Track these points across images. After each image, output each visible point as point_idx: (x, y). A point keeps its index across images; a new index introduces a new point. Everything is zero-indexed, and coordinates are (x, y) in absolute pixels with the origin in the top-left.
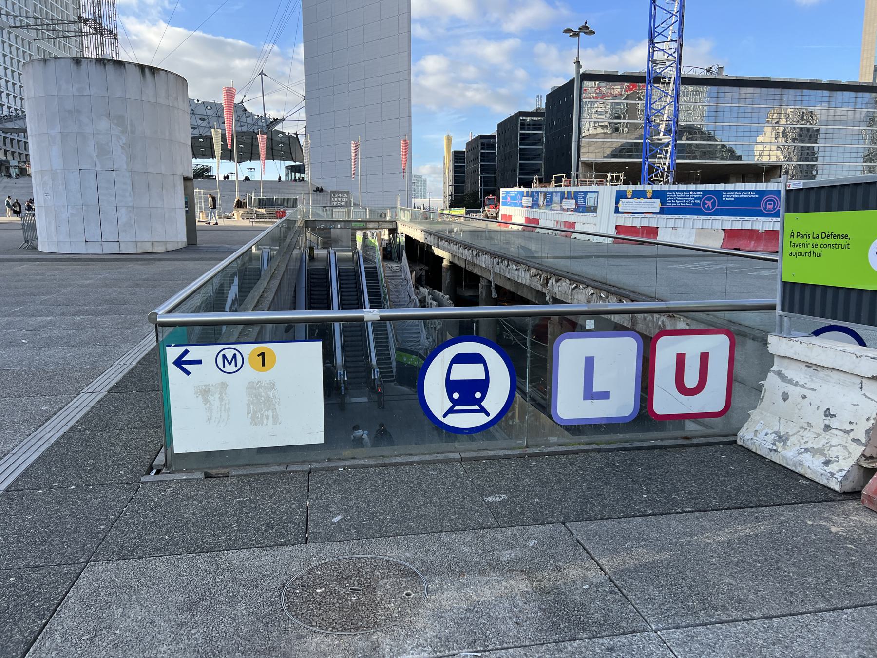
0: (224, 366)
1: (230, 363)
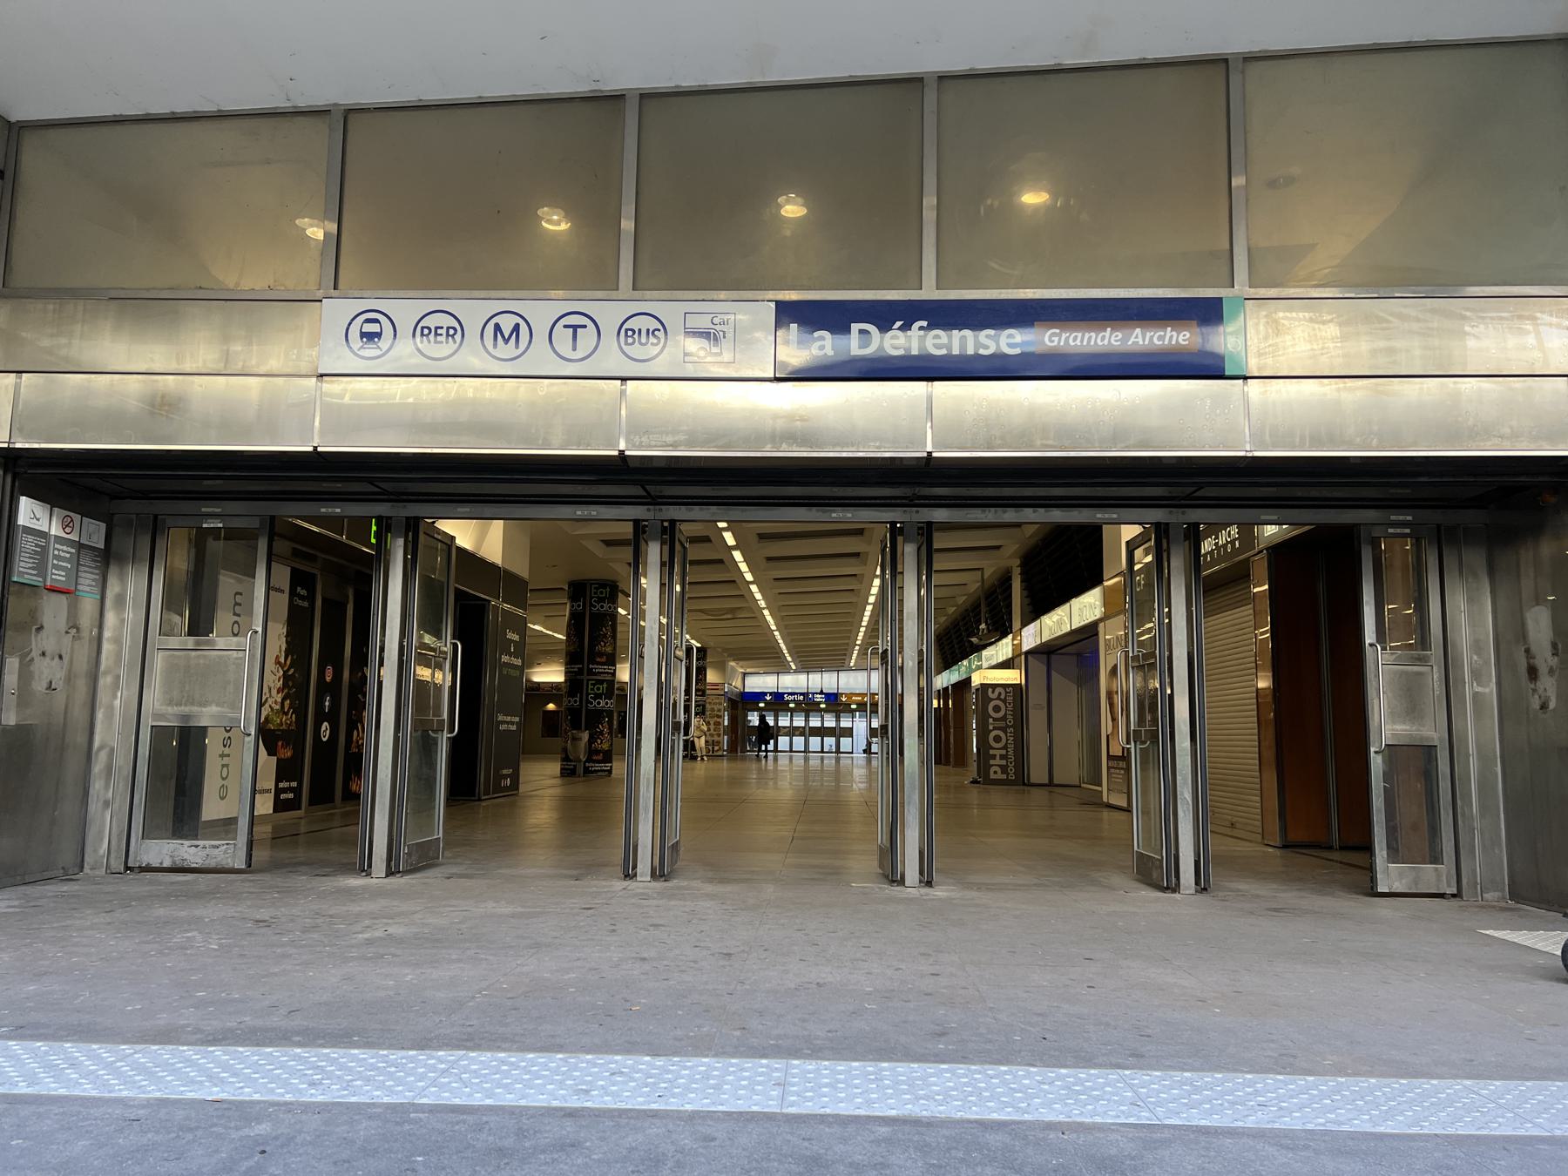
0: (495, 346)
1: (506, 341)
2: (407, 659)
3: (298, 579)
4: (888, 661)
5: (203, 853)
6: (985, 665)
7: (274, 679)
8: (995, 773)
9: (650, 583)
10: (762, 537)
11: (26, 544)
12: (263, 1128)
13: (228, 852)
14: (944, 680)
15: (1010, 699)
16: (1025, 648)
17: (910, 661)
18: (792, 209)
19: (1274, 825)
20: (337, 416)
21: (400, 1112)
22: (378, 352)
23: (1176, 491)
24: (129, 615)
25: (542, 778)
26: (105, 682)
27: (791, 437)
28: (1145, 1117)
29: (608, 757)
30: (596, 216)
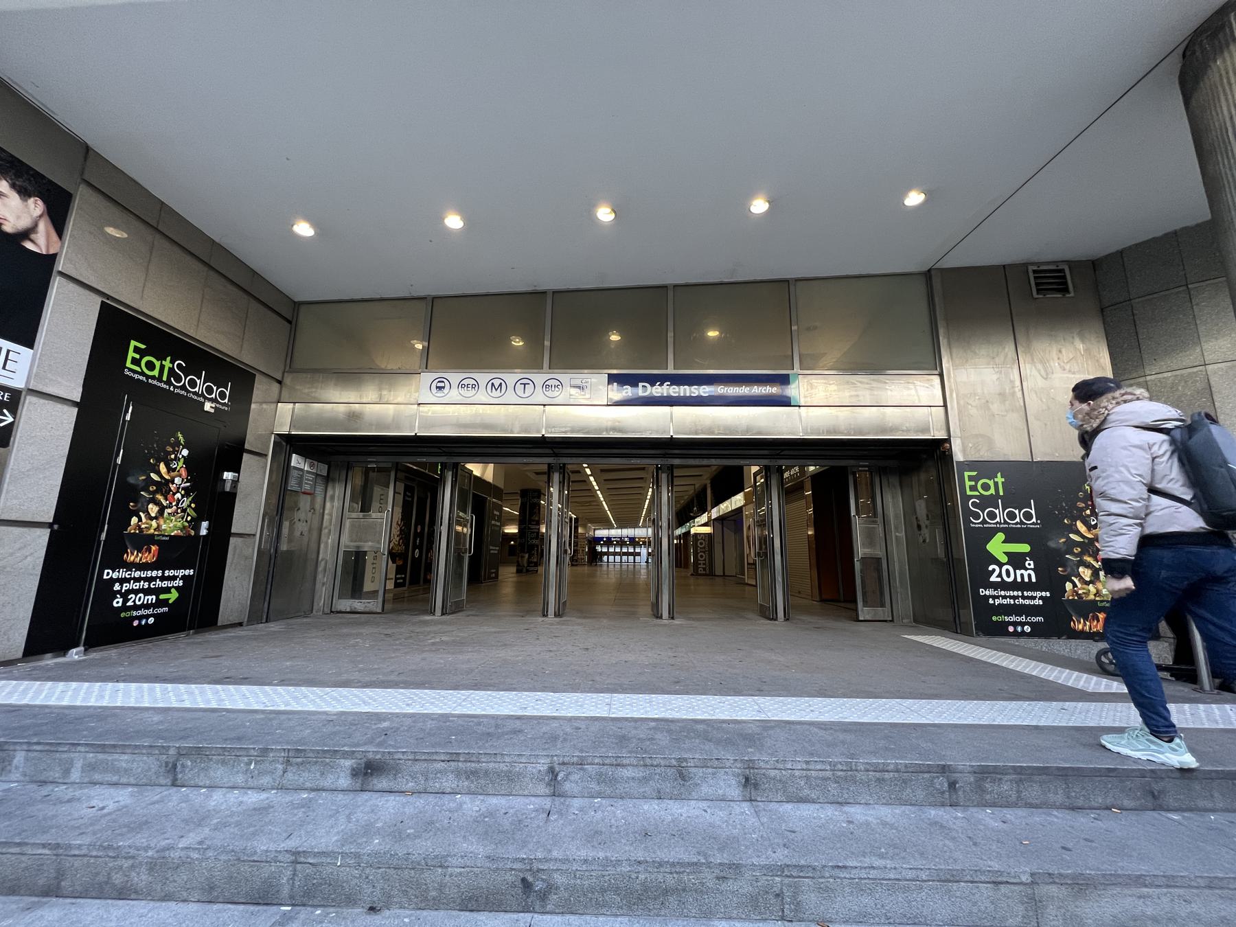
2: (451, 522)
3: (407, 488)
4: (655, 524)
7: (396, 531)
8: (701, 571)
9: (554, 490)
10: (602, 471)
11: (294, 473)
12: (386, 724)
13: (374, 605)
14: (679, 532)
17: (665, 524)
18: (615, 337)
19: (816, 591)
20: (426, 422)
21: (445, 717)
22: (1139, 749)
23: (773, 452)
25: (508, 574)
26: (325, 531)
27: (614, 429)
28: (763, 717)
29: (536, 564)
30: (534, 340)
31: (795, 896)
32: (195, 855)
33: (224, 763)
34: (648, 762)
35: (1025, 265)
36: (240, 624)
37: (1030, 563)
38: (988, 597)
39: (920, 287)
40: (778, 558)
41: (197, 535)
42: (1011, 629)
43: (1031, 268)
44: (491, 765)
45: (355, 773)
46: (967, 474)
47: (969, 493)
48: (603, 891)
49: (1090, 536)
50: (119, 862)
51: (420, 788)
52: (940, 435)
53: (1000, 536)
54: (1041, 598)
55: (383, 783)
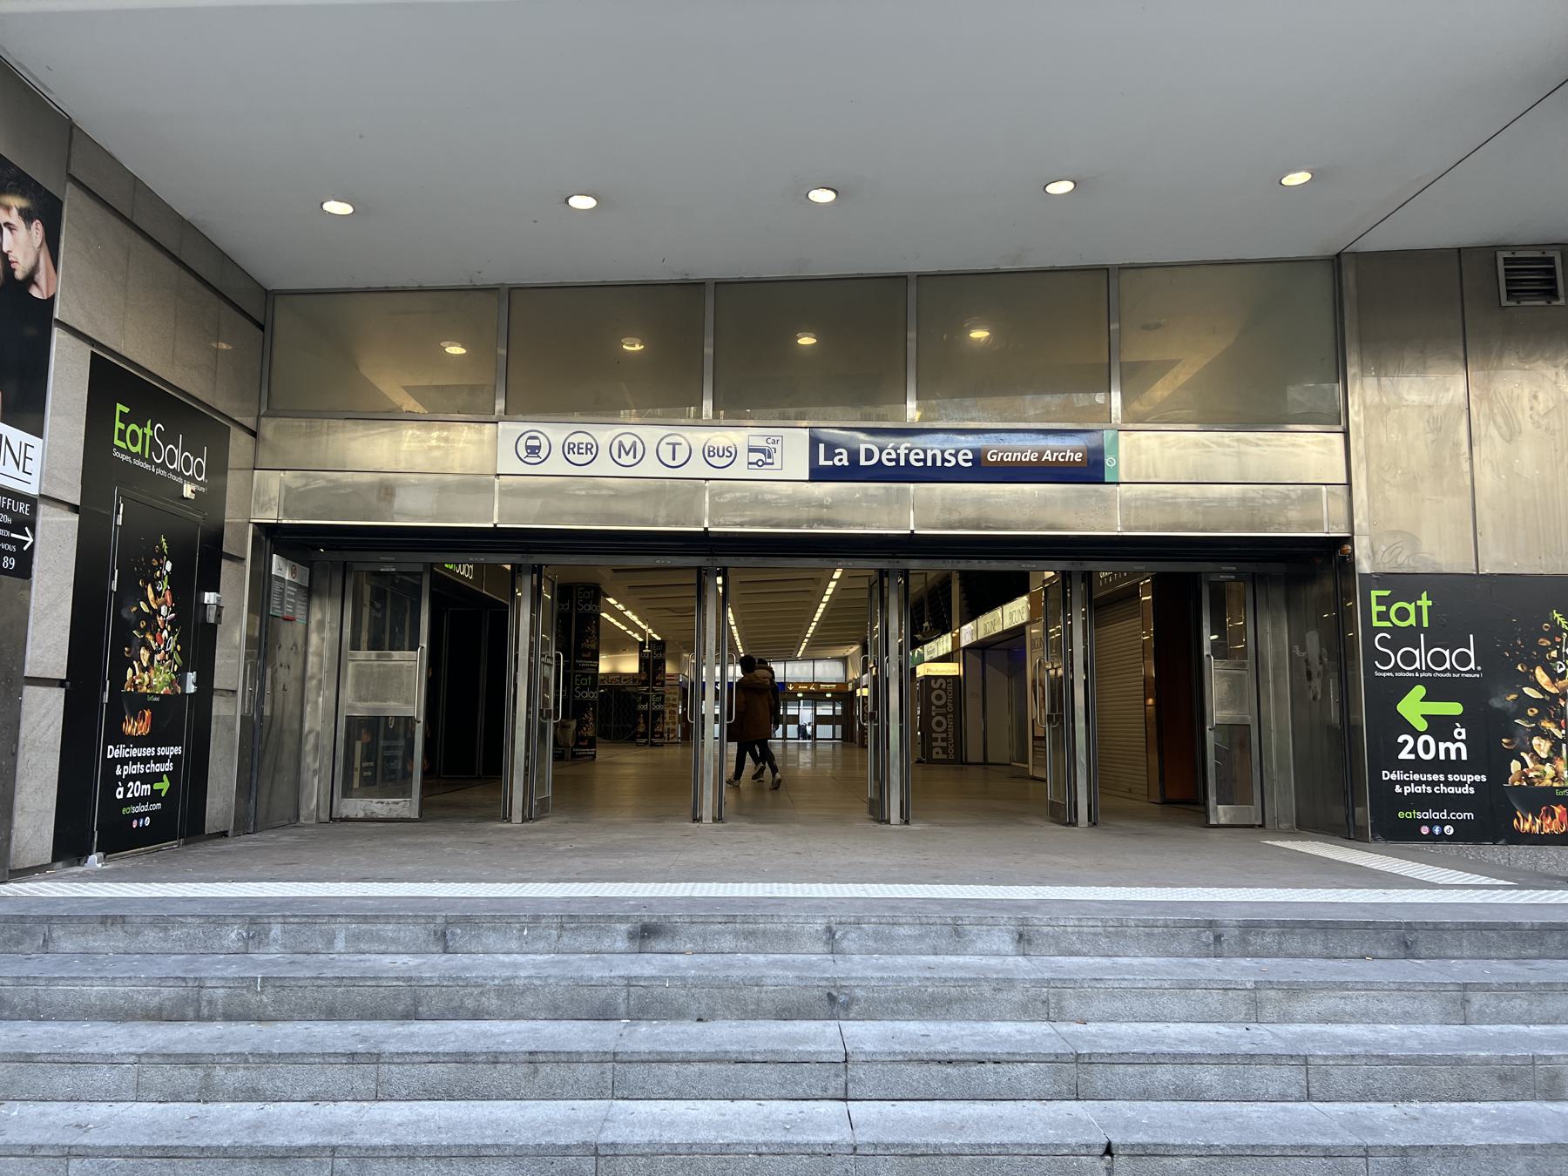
5: (386, 808)
6: (927, 658)
8: (937, 754)
11: (276, 587)
15: (950, 689)
16: (963, 644)
19: (1156, 788)
24: (327, 634)
31: (1058, 1003)
32: (538, 982)
33: (494, 929)
34: (924, 920)
35: (1491, 250)
36: (224, 834)
37: (1460, 732)
38: (1392, 783)
39: (1320, 284)
40: (1080, 724)
41: (184, 693)
42: (1425, 830)
43: (1502, 255)
44: (769, 926)
45: (632, 936)
46: (1374, 594)
47: (1376, 623)
48: (897, 1001)
49: (1553, 690)
50: (469, 990)
51: (699, 948)
52: (1340, 532)
53: (1420, 691)
54: (1473, 784)
55: (661, 945)
